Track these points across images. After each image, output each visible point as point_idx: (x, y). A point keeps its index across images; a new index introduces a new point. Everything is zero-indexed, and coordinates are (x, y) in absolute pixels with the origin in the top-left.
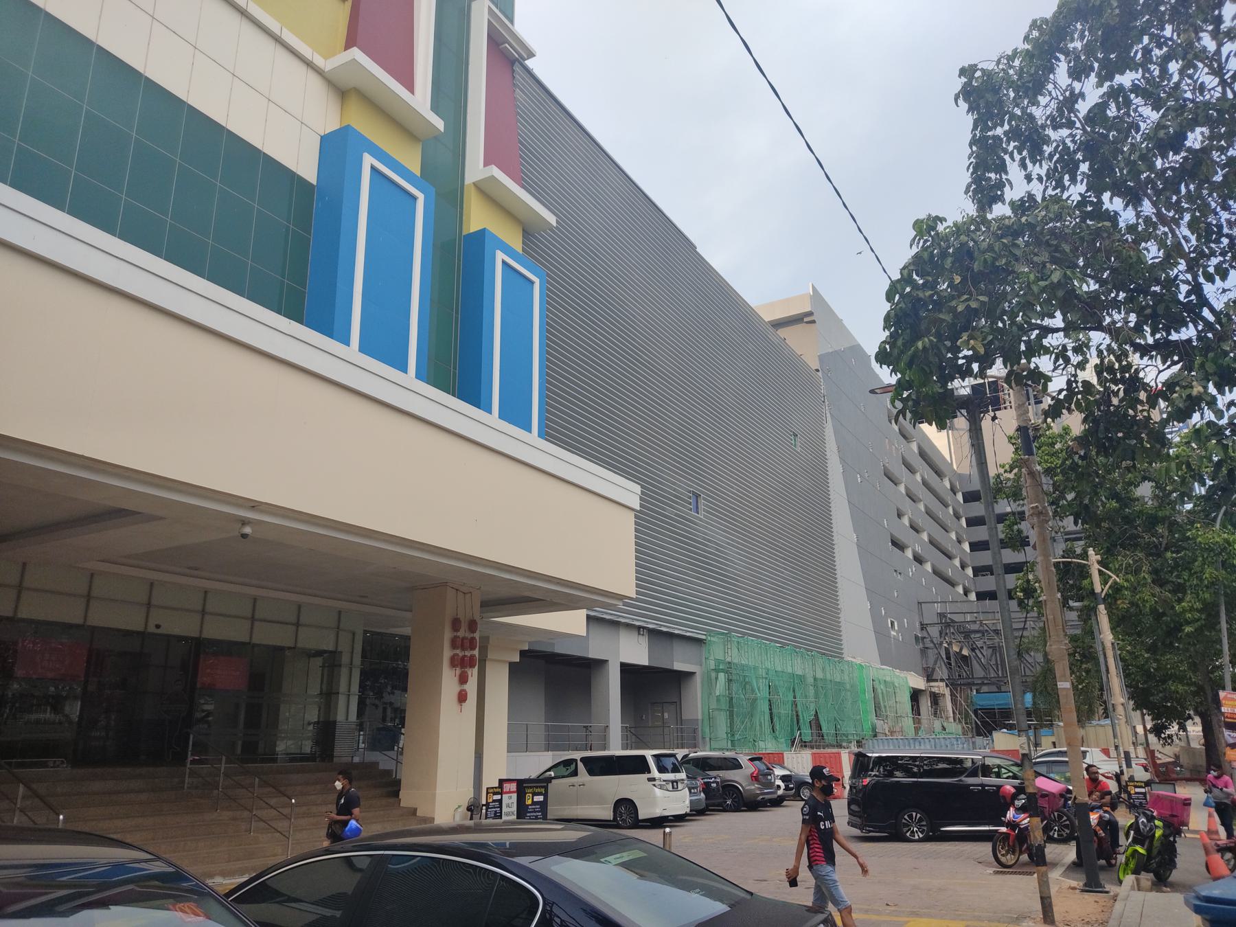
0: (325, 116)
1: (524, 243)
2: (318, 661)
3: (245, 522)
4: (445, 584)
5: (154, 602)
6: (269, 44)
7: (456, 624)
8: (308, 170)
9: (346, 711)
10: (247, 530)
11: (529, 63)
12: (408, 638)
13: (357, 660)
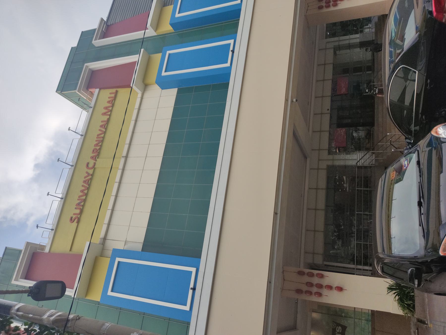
0: (155, 91)
1: (168, 5)
2: (338, 52)
3: (292, 101)
4: (305, 16)
5: (315, 187)
6: (116, 213)
7: (320, 8)
8: (174, 92)
9: (356, 38)
10: (294, 100)
11: (105, 19)
12: (327, 24)
13: (336, 39)
